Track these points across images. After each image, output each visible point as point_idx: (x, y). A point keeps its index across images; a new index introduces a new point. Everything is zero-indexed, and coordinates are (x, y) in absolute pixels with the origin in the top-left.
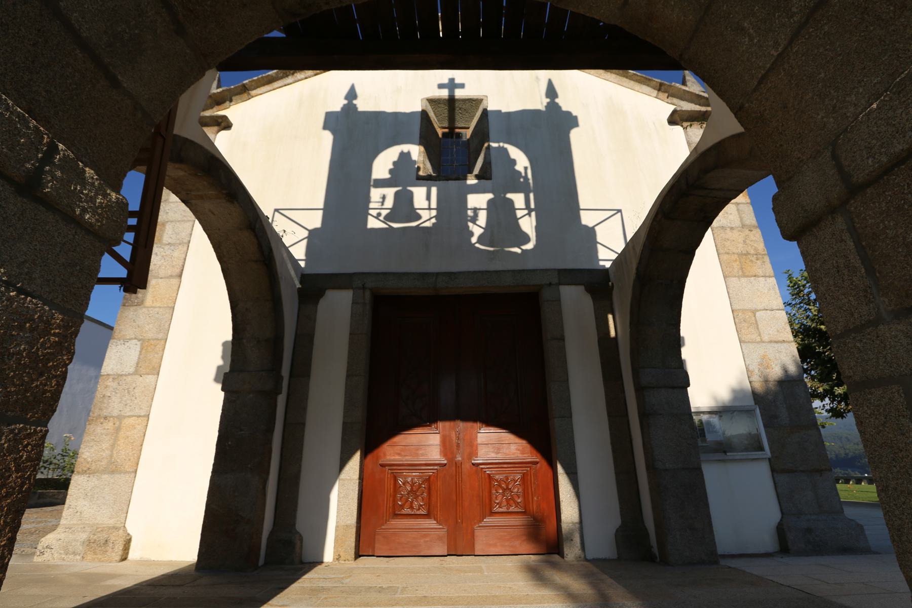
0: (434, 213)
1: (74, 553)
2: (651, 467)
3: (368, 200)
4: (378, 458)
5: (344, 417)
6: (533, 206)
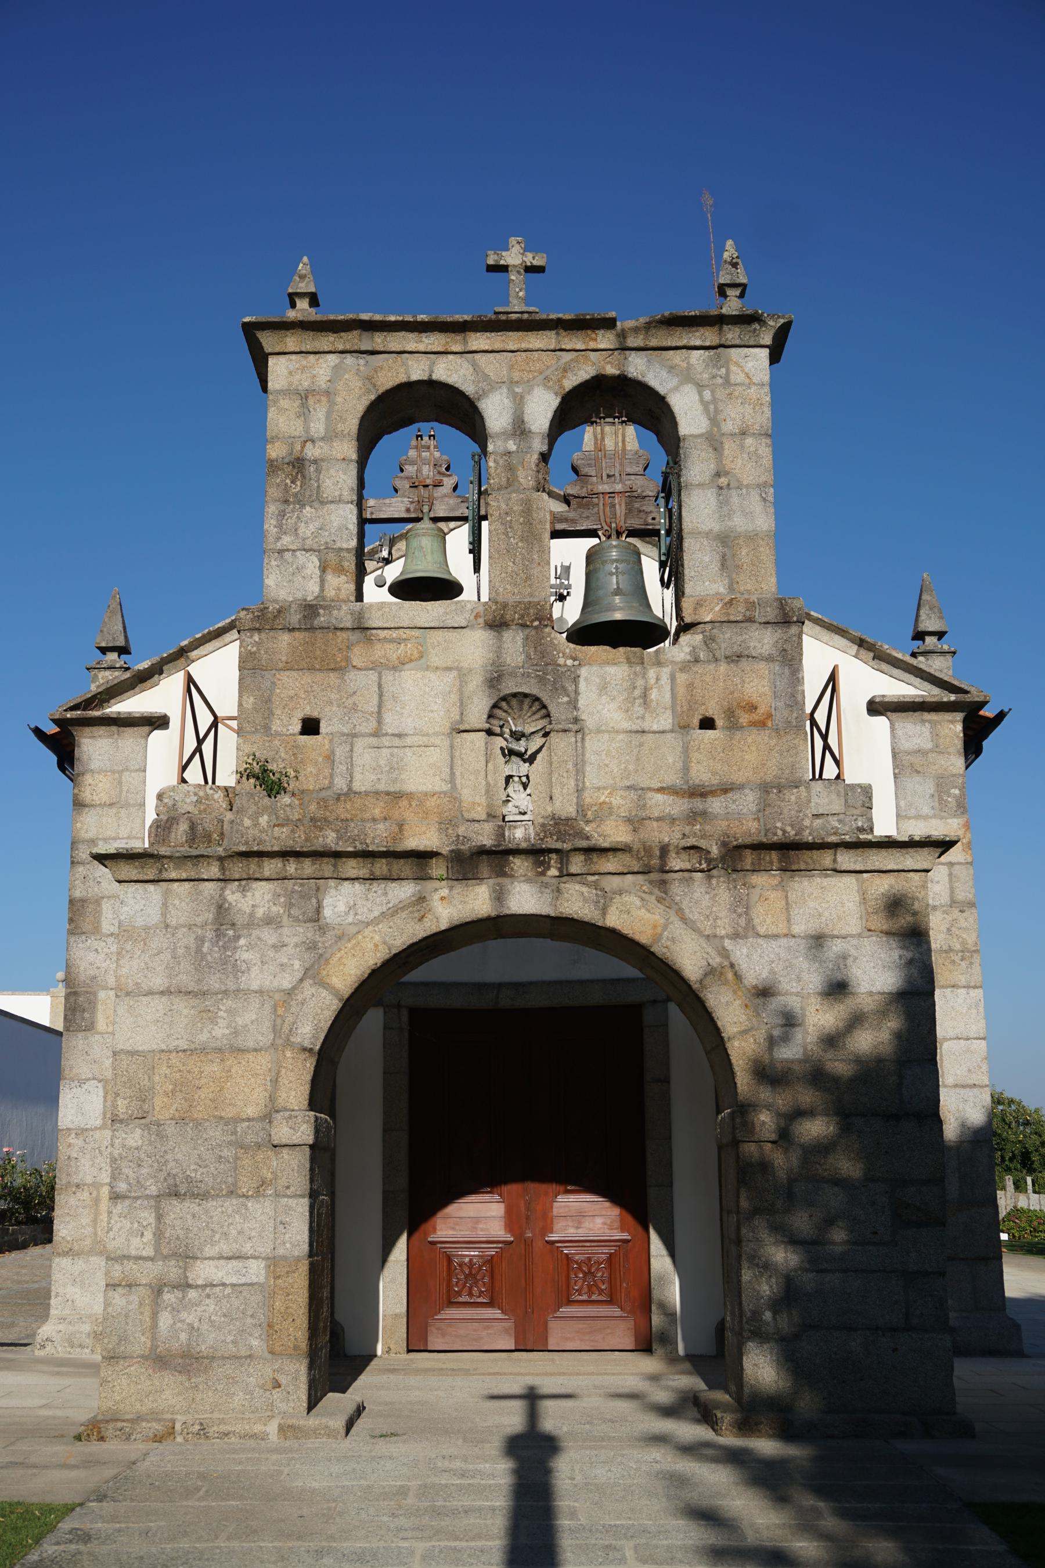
1: (81, 1346)
5: (384, 1184)
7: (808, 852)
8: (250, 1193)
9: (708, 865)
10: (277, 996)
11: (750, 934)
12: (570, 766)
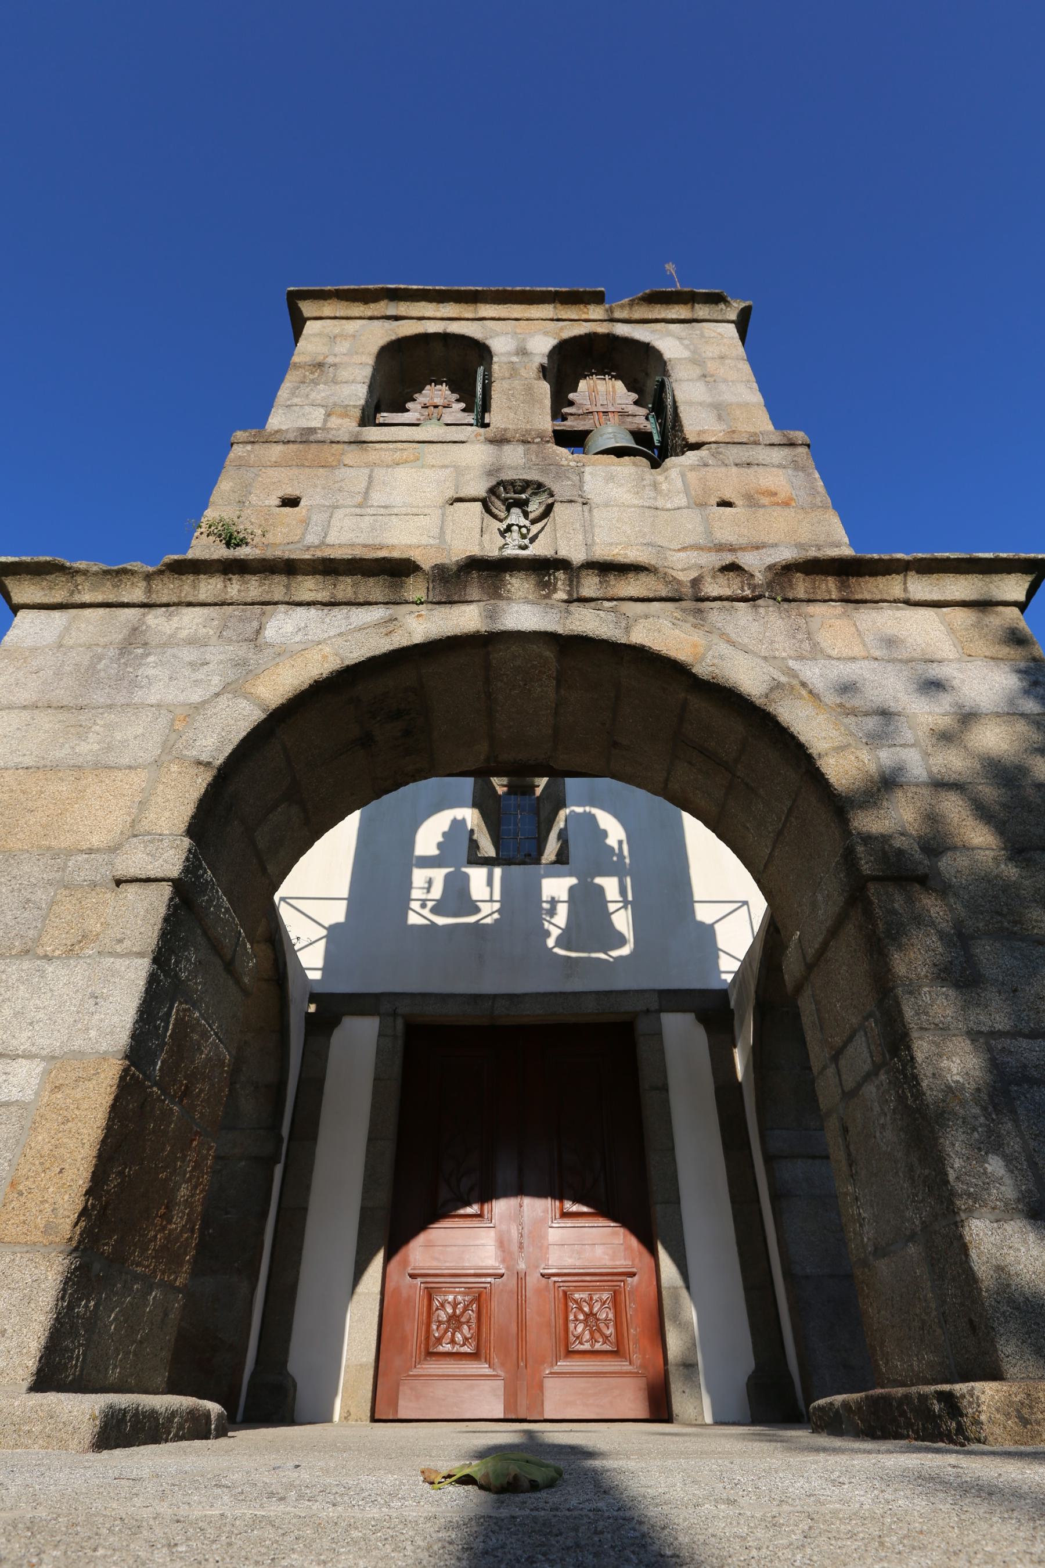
0: (497, 906)
2: (787, 1274)
3: (409, 886)
4: (405, 1263)
5: (363, 1199)
6: (630, 898)
7: (872, 579)
8: (57, 953)
9: (753, 591)
10: (178, 711)
11: (819, 656)
12: (578, 526)
